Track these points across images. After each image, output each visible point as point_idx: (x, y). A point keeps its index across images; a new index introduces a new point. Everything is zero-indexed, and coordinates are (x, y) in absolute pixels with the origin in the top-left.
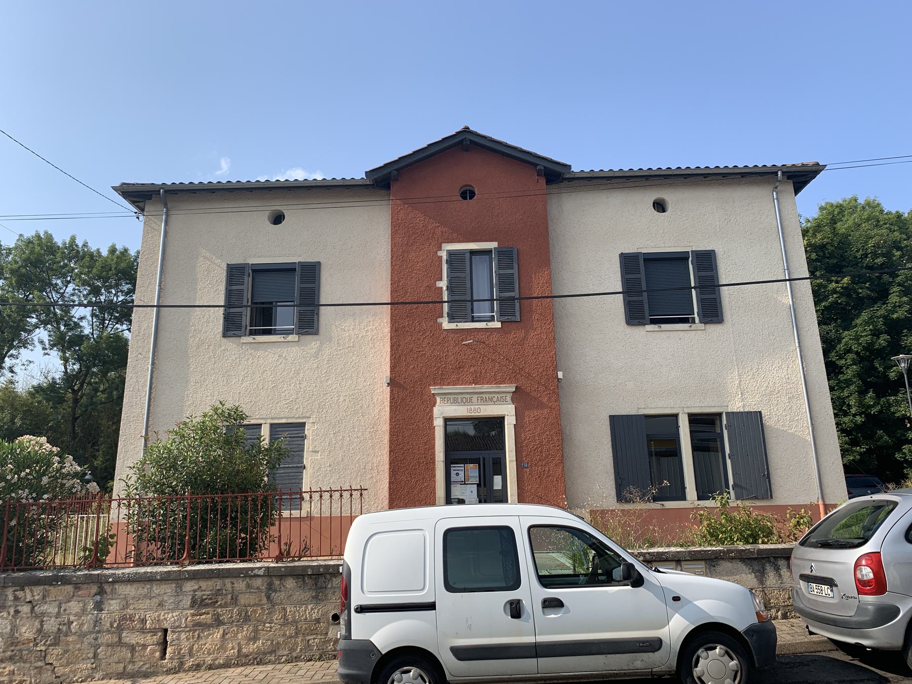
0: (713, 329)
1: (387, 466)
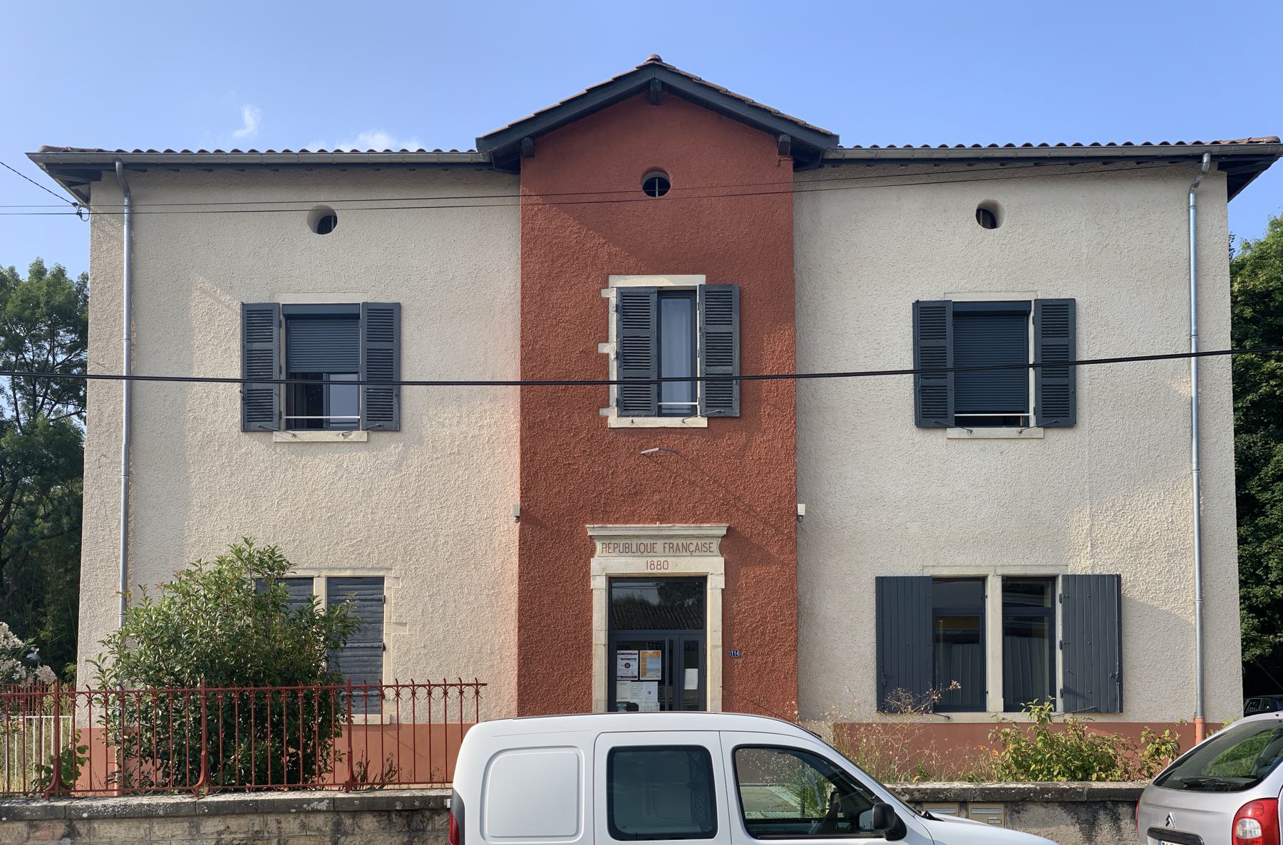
0: (1059, 437)
1: (515, 650)
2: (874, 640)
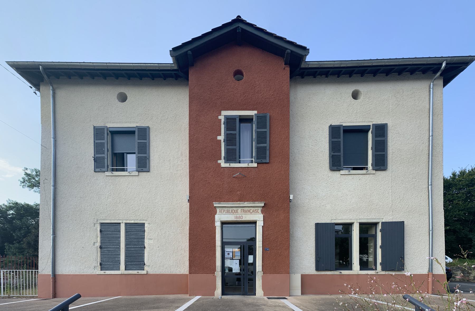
2: (314, 245)
